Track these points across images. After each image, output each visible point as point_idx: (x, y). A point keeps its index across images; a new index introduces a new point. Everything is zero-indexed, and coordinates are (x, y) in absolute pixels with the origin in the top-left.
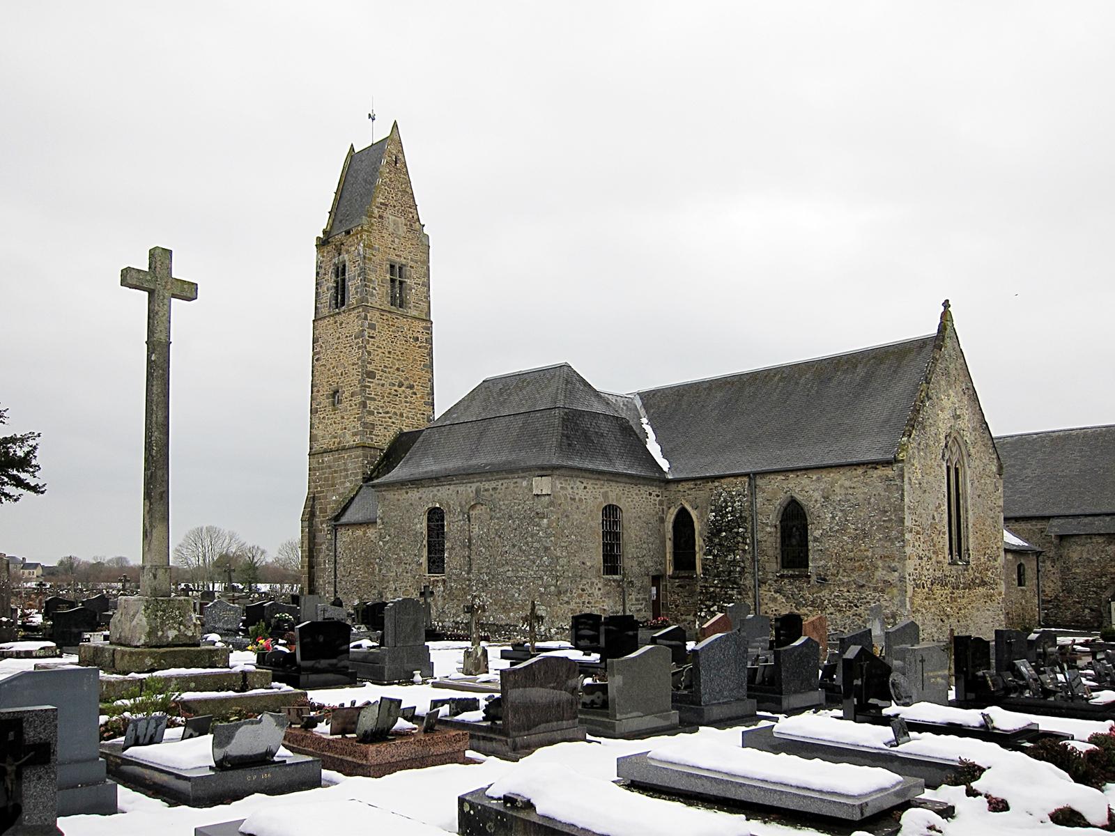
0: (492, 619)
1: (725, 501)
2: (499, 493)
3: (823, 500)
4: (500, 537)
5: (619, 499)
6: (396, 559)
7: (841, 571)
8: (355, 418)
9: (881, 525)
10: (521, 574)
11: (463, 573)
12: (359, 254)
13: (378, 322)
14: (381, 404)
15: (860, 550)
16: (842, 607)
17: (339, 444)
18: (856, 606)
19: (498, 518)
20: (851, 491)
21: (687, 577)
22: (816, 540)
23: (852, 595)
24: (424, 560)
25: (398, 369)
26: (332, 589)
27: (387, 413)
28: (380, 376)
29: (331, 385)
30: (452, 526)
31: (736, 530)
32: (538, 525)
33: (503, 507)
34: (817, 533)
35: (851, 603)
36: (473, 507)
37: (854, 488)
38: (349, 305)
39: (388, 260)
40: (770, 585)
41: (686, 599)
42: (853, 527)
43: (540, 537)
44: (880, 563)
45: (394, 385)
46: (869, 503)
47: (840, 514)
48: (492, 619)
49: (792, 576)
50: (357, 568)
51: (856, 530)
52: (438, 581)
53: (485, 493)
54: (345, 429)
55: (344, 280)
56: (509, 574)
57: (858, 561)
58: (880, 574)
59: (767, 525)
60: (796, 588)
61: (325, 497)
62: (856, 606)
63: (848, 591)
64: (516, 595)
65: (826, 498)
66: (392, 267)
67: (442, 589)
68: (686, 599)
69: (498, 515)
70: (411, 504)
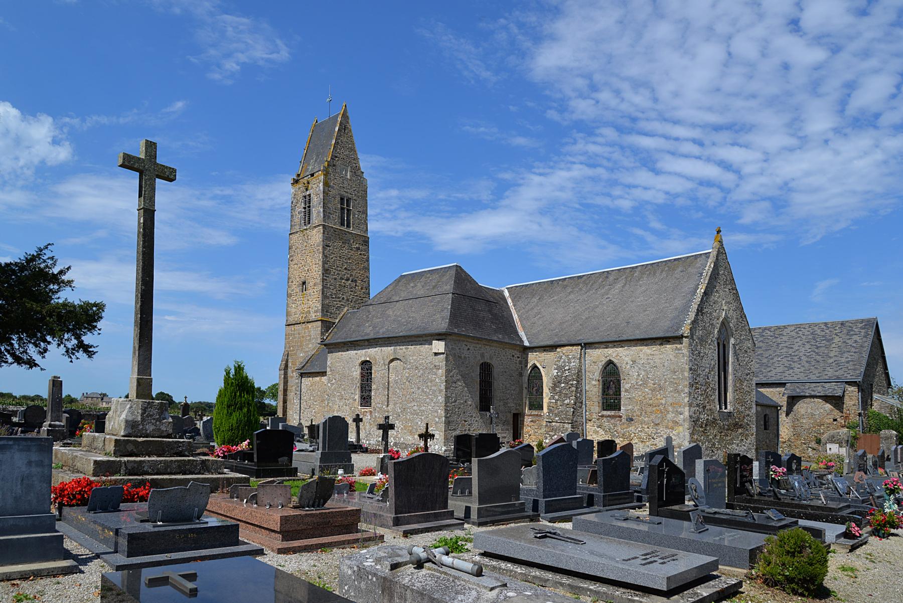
0: (402, 440)
1: (564, 362)
2: (410, 351)
3: (632, 363)
4: (409, 382)
5: (491, 358)
6: (339, 396)
7: (643, 413)
9: (671, 382)
10: (423, 408)
11: (384, 407)
12: (320, 190)
13: (332, 236)
14: (334, 292)
15: (657, 399)
16: (644, 438)
17: (305, 318)
18: (653, 438)
19: (408, 369)
20: (650, 357)
21: (537, 415)
22: (626, 391)
23: (650, 431)
24: (357, 397)
25: (346, 269)
26: (298, 417)
27: (339, 298)
28: (334, 273)
29: (300, 277)
30: (377, 373)
31: (571, 382)
32: (436, 374)
33: (412, 361)
34: (627, 386)
35: (650, 436)
36: (392, 361)
37: (653, 355)
38: (313, 224)
39: (339, 194)
40: (594, 422)
41: (536, 430)
42: (652, 382)
43: (437, 383)
44: (670, 409)
45: (343, 279)
46: (664, 366)
47: (643, 373)
48: (402, 440)
49: (609, 416)
51: (654, 384)
53: (400, 351)
54: (310, 308)
55: (309, 207)
56: (415, 408)
57: (655, 406)
58: (670, 416)
59: (593, 379)
60: (612, 424)
61: (295, 354)
62: (653, 438)
63: (648, 428)
64: (419, 423)
65: (634, 362)
66: (342, 199)
67: (369, 417)
68: (536, 430)
69: (408, 367)
70: (350, 358)
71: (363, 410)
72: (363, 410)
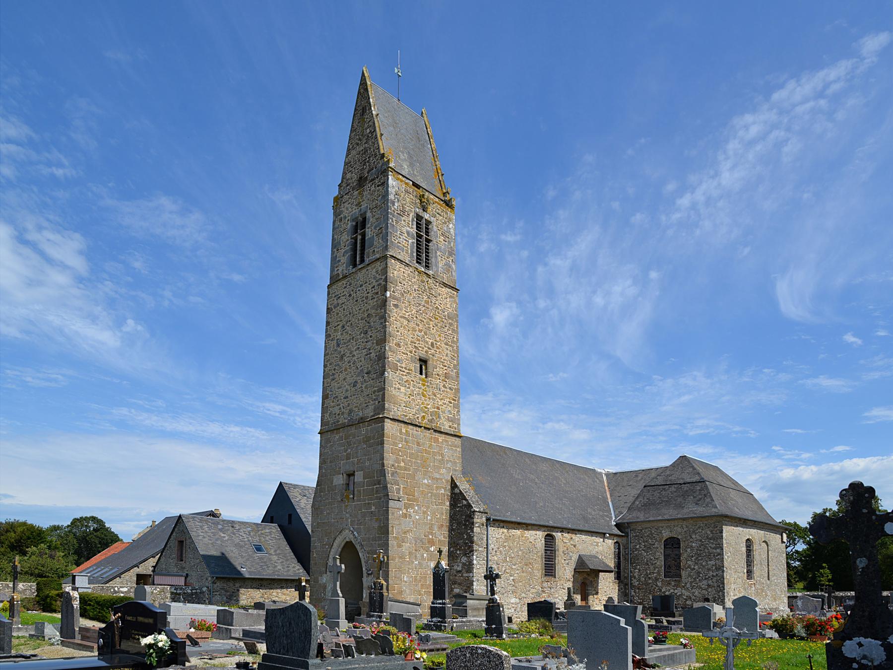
6: (733, 569)
8: (451, 403)
50: (514, 567)
52: (752, 584)
71: (750, 583)
72: (750, 583)
